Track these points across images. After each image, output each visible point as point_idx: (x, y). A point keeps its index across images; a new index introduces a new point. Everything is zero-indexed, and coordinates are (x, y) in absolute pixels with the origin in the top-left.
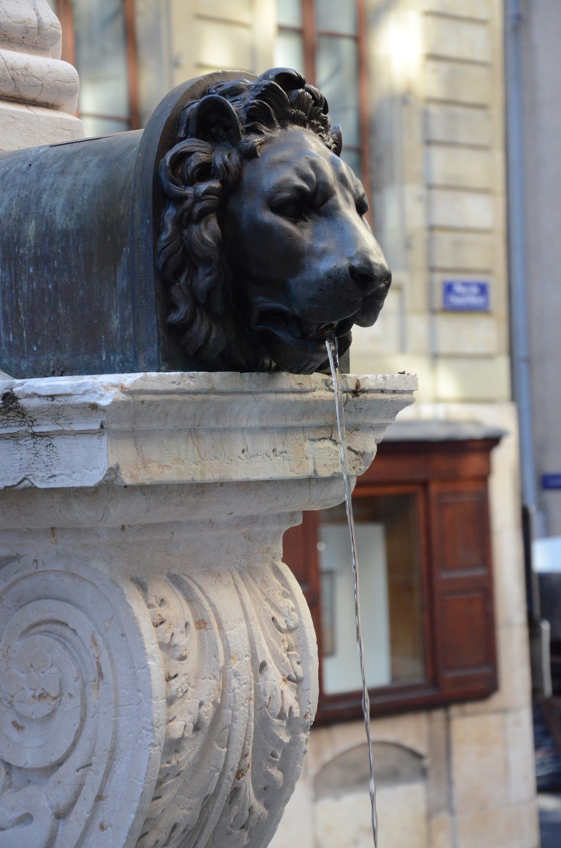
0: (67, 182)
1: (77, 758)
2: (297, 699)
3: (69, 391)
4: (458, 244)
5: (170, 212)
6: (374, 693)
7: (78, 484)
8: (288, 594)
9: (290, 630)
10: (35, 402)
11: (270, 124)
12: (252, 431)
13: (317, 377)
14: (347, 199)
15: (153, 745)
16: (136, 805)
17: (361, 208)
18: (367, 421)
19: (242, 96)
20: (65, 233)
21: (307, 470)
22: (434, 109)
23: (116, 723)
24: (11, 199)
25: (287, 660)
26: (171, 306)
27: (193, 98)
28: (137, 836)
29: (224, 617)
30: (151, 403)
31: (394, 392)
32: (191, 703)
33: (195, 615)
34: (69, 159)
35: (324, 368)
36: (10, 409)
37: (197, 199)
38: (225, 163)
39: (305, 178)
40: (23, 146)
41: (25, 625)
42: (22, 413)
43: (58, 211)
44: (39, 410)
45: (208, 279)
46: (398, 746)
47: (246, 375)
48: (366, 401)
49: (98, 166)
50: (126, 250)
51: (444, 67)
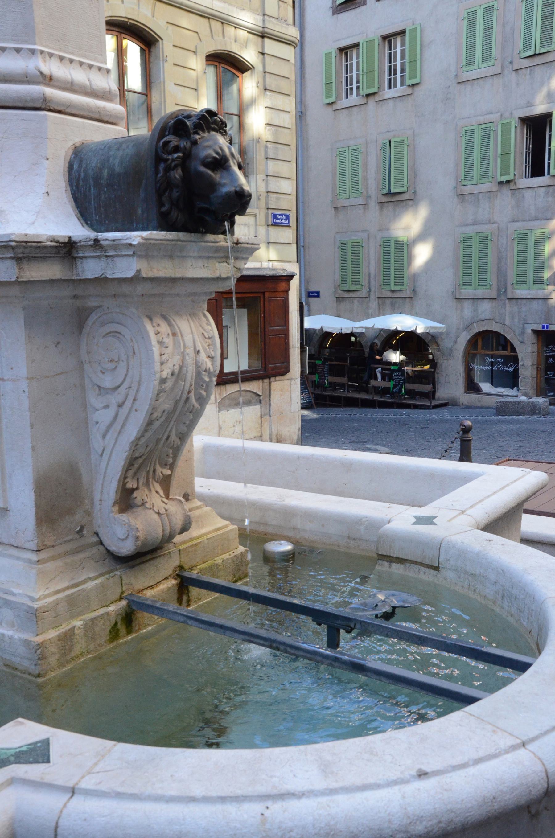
0: (120, 153)
1: (126, 385)
2: (212, 365)
3: (120, 238)
4: (278, 199)
5: (162, 166)
6: (243, 372)
7: (124, 277)
8: (209, 324)
9: (209, 338)
10: (107, 243)
11: (203, 131)
12: (195, 257)
13: (221, 236)
14: (234, 163)
15: (155, 380)
16: (149, 403)
17: (240, 167)
18: (241, 255)
19: (192, 119)
20: (119, 174)
21: (217, 275)
22: (269, 145)
23: (140, 372)
24: (97, 161)
25: (208, 350)
26: (162, 205)
27: (171, 119)
28: (149, 414)
29: (183, 332)
30: (154, 244)
31: (252, 244)
32: (170, 365)
33: (171, 330)
34: (121, 144)
35: (224, 233)
36: (97, 245)
37: (173, 160)
38: (185, 146)
39: (217, 153)
40: (102, 139)
41: (104, 333)
42: (101, 247)
43: (116, 165)
44: (109, 246)
45: (177, 194)
46: (251, 392)
47: (193, 234)
48: (241, 247)
49: (133, 146)
50: (144, 181)
51: (273, 128)
